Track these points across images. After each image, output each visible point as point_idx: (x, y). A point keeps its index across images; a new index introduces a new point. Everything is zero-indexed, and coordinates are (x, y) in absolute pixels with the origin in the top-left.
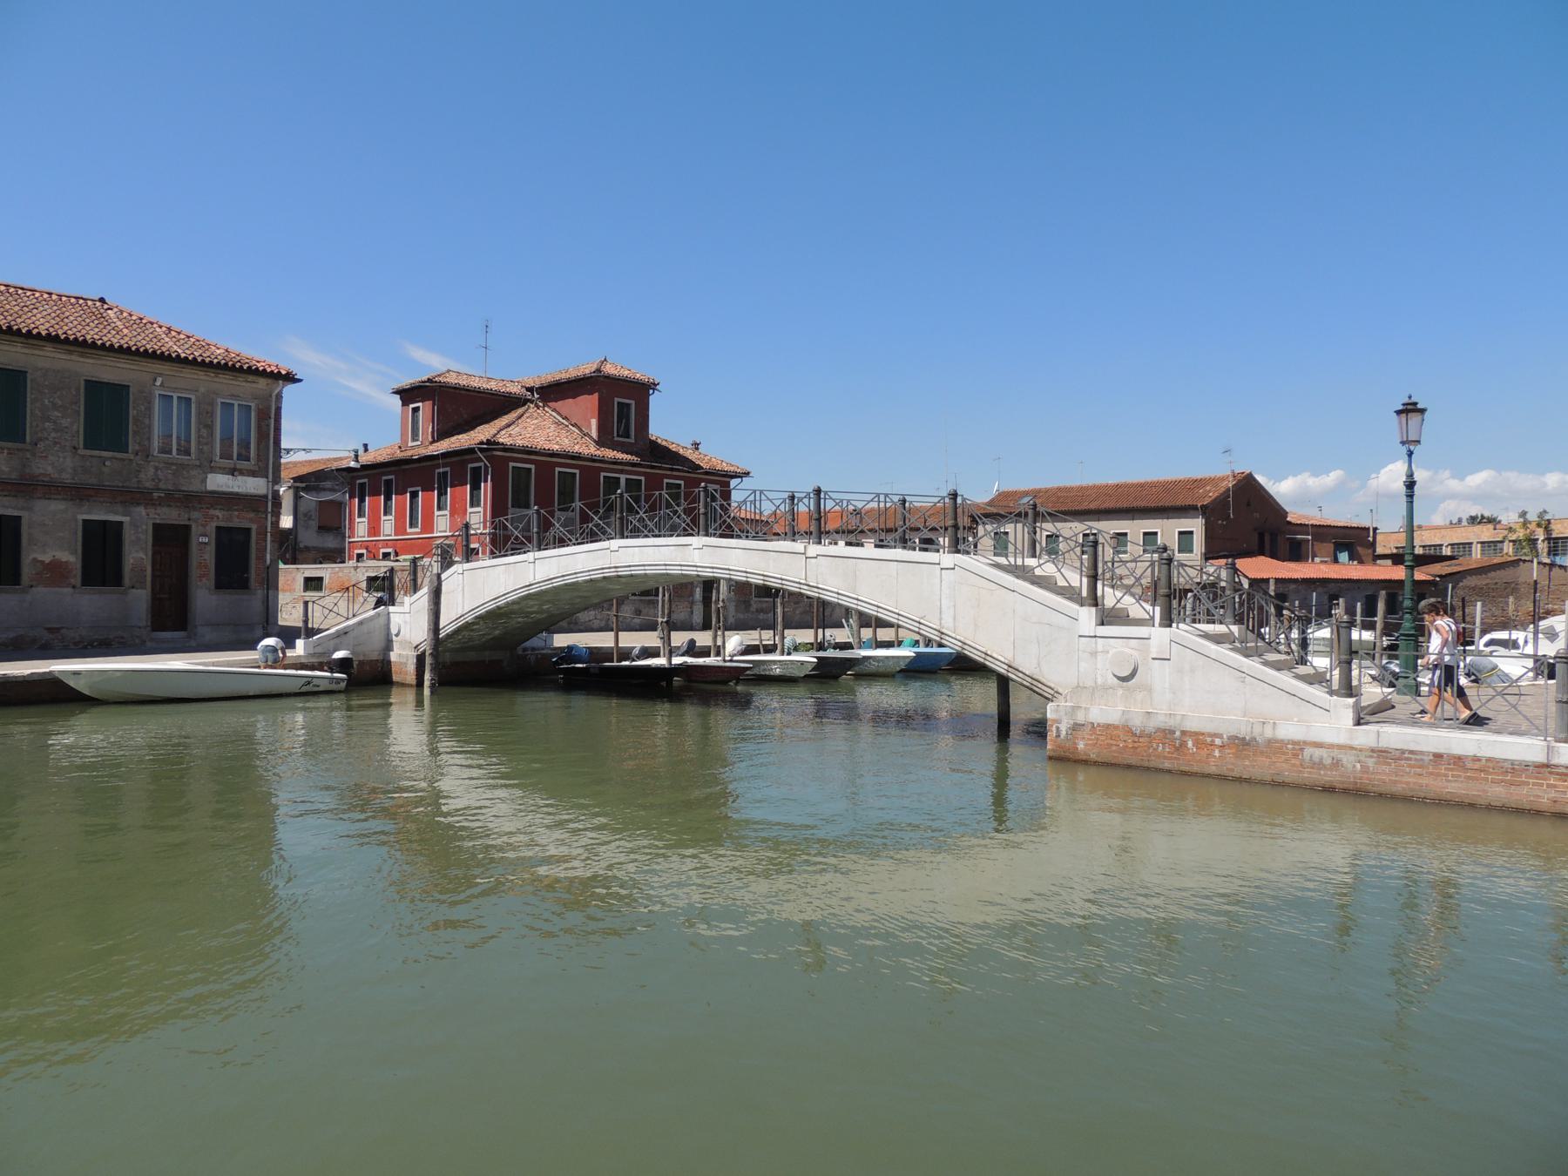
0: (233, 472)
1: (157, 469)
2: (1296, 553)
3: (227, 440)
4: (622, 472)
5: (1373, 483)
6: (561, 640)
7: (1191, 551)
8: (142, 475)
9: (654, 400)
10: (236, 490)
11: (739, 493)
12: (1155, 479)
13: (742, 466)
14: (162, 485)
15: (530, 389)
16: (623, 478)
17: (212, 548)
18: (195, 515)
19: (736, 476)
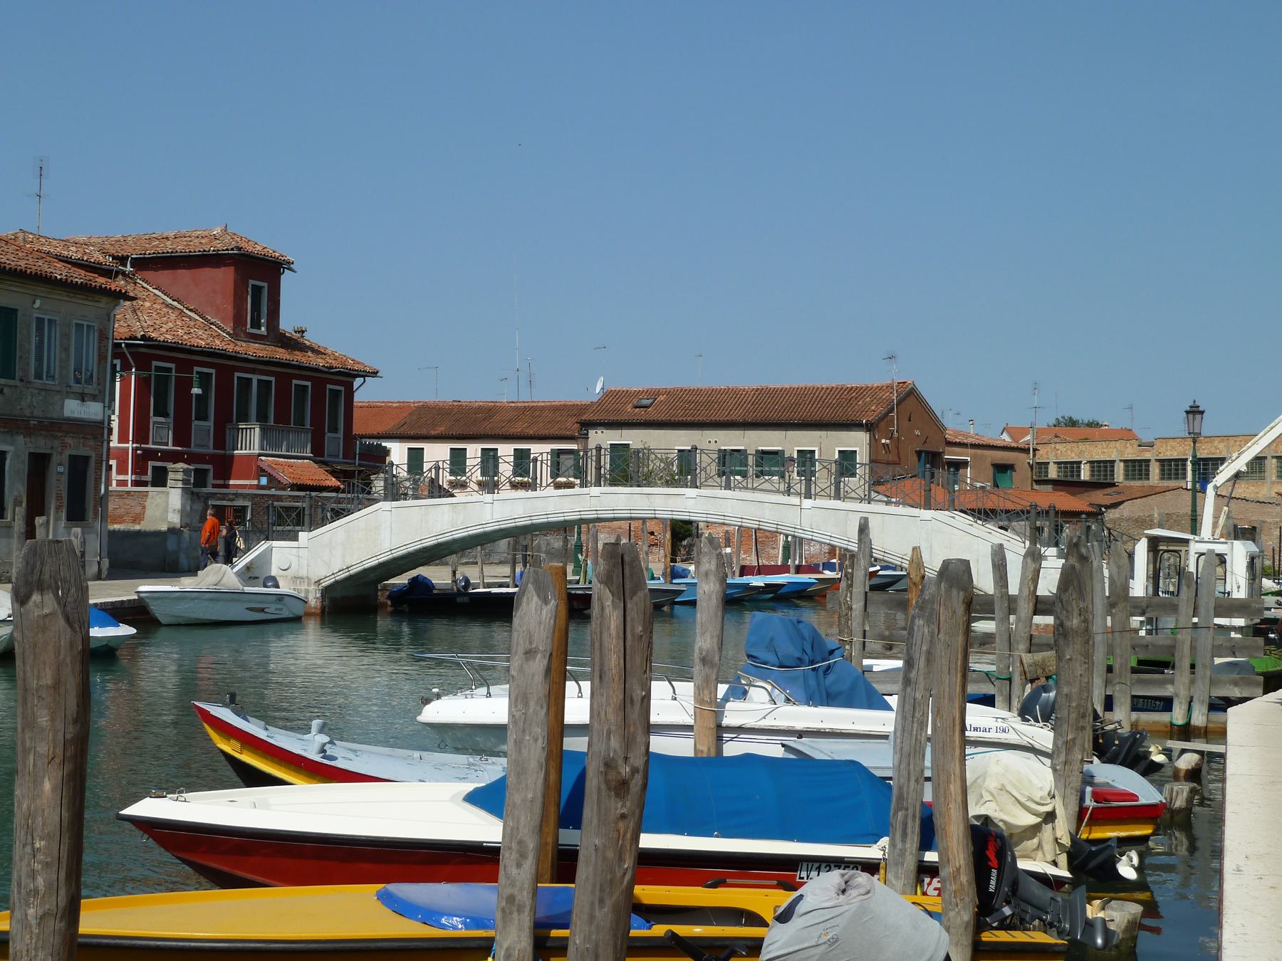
0: (83, 398)
1: (32, 395)
2: (284, 489)
3: (78, 369)
4: (253, 371)
5: (421, 718)
6: (391, 581)
7: (154, 467)
8: (23, 403)
9: (286, 279)
10: (83, 416)
11: (365, 393)
12: (802, 385)
13: (369, 363)
14: (36, 413)
15: (122, 260)
16: (255, 378)
17: (65, 479)
18: (57, 443)
19: (365, 374)
